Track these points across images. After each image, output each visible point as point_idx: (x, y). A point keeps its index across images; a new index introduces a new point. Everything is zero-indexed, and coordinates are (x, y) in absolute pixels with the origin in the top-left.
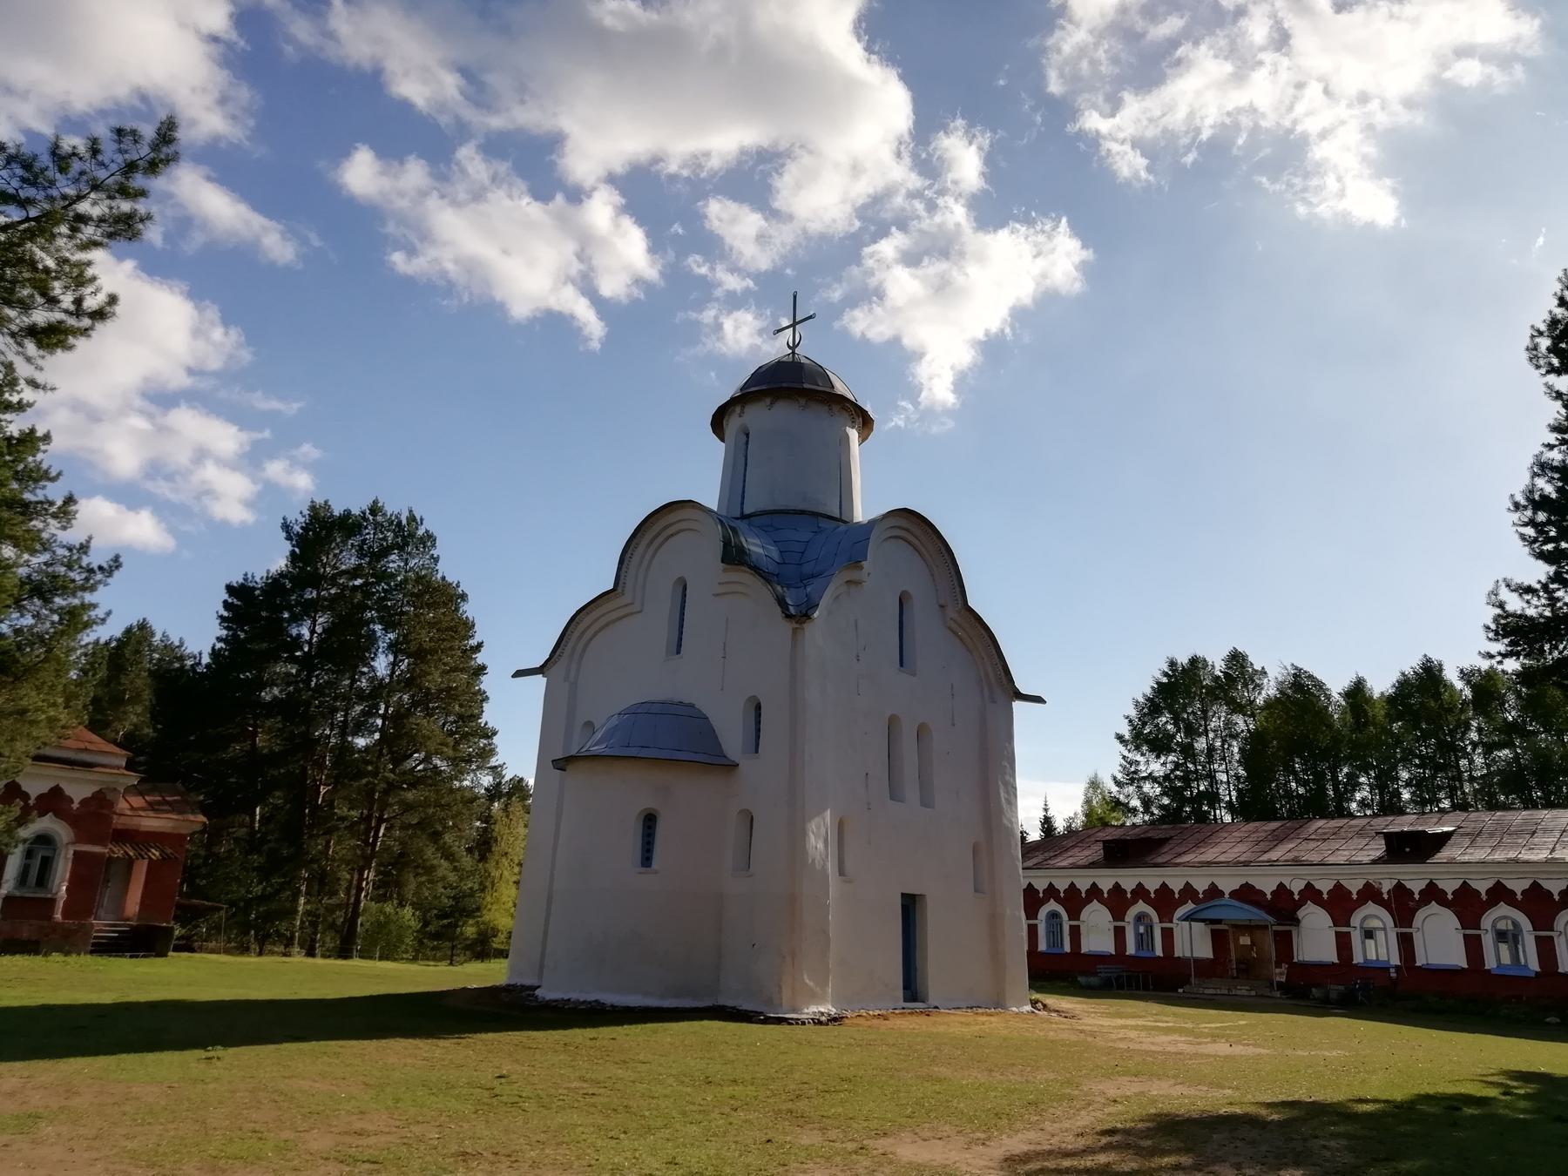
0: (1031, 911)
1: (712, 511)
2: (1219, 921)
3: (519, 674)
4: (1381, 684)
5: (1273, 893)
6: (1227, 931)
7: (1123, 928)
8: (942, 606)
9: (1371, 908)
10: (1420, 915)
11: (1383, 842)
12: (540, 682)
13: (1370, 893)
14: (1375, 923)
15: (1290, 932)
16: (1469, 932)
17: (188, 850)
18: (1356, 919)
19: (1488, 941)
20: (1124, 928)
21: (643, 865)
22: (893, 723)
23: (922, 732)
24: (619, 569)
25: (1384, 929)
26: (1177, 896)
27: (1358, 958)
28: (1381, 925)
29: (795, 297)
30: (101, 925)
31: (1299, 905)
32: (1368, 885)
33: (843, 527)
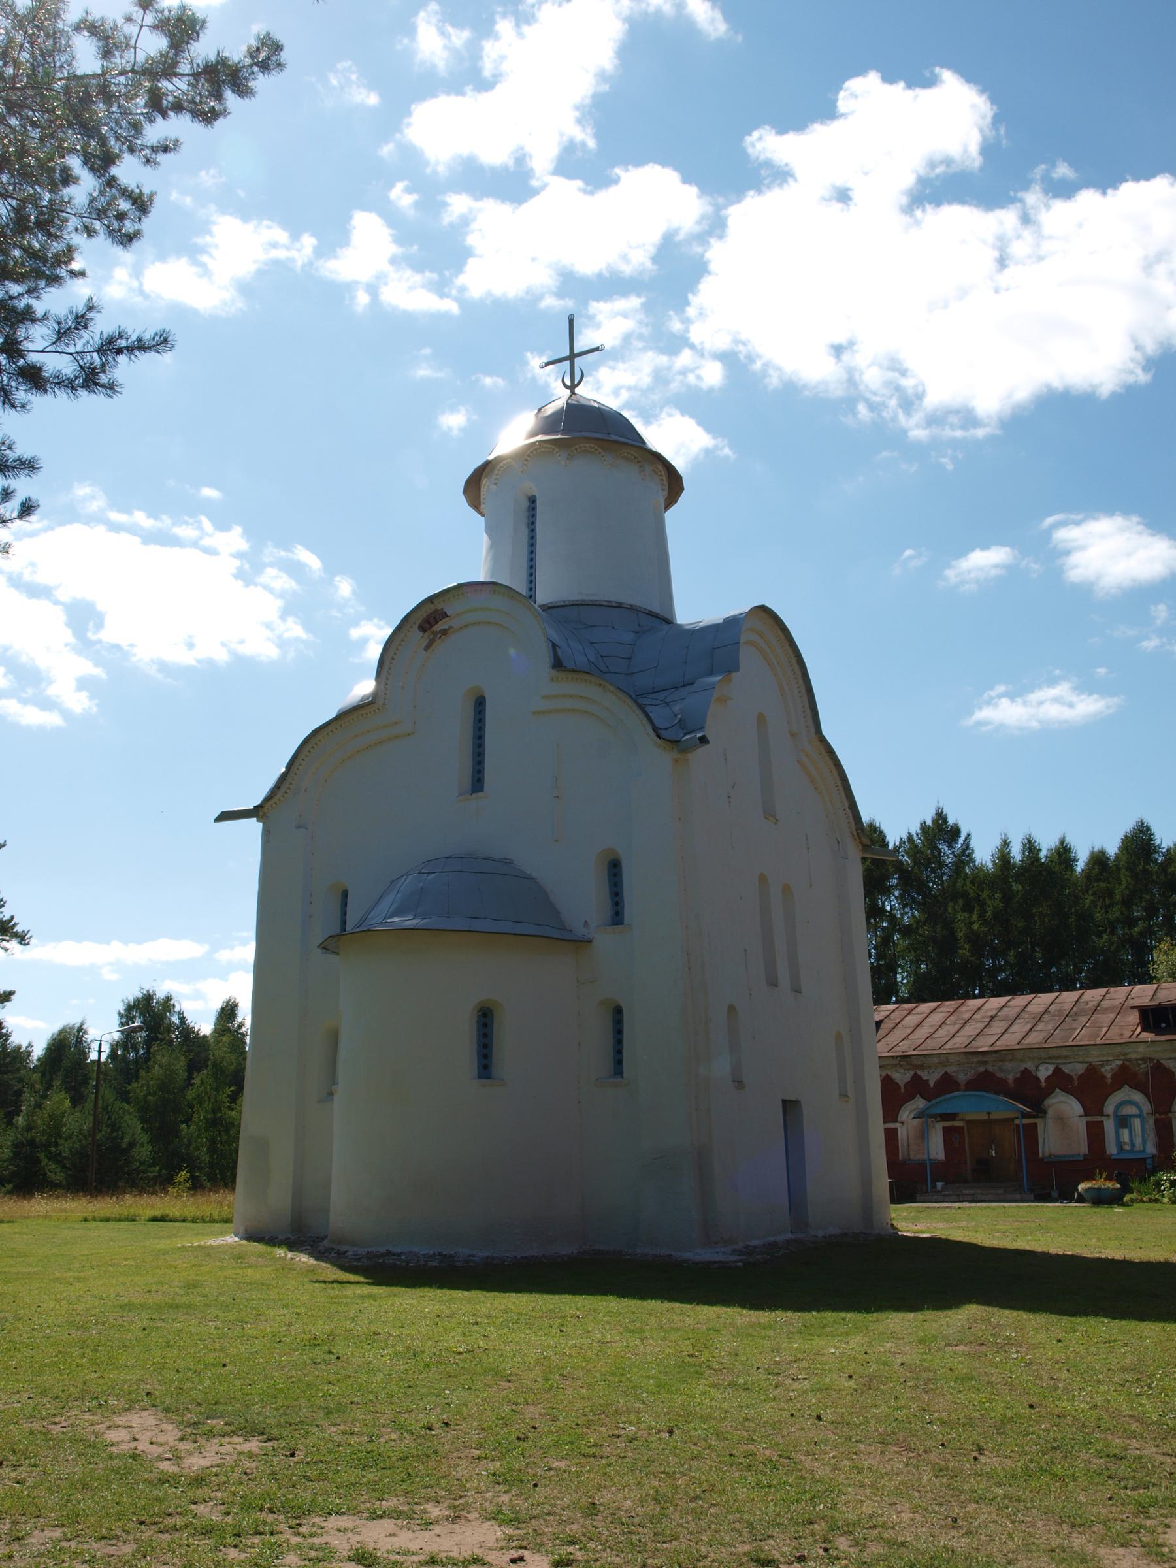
0: (891, 1110)
1: (522, 595)
2: (952, 1117)
3: (225, 816)
4: (1112, 848)
5: (1016, 1080)
6: (963, 1127)
7: (1101, 1124)
8: (792, 735)
9: (1126, 1093)
10: (1049, 1102)
11: (1138, 1013)
12: (254, 827)
13: (1126, 1076)
14: (1130, 1110)
15: (1035, 1125)
16: (1090, 1119)
17: (146, 86)
18: (1109, 1108)
19: (1109, 1125)
20: (896, 1130)
21: (480, 1077)
22: (763, 879)
23: (773, 982)
24: (516, 591)
25: (1140, 1116)
26: (902, 1090)
27: (1112, 1149)
28: (1138, 1112)
29: (571, 322)
30: (640, 701)
31: (1048, 1092)
32: (1123, 1068)
33: (666, 627)
